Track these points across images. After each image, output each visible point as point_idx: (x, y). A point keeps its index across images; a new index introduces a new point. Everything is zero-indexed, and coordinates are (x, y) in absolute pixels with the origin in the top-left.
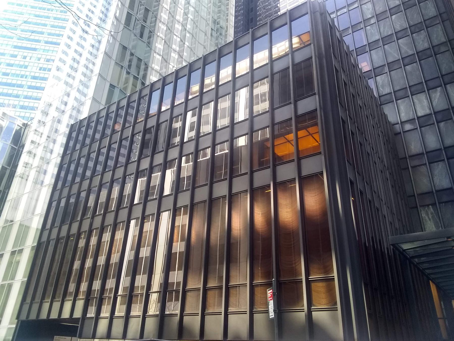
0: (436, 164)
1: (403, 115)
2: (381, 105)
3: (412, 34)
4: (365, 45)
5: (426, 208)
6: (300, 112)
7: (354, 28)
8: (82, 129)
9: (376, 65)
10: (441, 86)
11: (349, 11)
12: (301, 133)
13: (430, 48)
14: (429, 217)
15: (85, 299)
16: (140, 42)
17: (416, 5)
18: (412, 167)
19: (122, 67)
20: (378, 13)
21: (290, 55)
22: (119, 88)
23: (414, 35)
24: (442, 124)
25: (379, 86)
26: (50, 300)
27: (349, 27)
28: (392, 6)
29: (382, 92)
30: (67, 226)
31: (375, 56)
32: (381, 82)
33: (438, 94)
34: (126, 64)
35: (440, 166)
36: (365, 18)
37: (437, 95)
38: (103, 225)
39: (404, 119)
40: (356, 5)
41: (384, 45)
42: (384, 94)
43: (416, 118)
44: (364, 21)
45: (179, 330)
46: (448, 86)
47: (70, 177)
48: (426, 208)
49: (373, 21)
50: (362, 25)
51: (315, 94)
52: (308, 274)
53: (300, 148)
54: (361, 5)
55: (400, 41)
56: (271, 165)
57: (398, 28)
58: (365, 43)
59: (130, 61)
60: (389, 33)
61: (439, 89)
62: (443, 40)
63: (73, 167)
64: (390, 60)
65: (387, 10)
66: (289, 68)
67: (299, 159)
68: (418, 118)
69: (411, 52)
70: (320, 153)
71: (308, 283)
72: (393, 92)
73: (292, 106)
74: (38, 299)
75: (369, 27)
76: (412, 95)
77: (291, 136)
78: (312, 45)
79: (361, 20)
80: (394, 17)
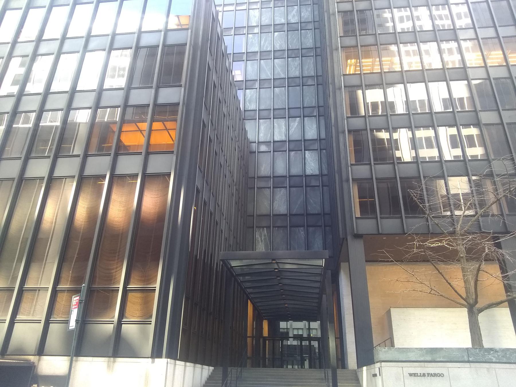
1: (261, 135)
2: (244, 119)
3: (288, 58)
6: (161, 101)
7: (237, 30)
9: (249, 78)
10: (300, 117)
11: (236, 10)
12: (156, 125)
13: (299, 77)
17: (298, 30)
20: (263, 24)
21: (163, 33)
23: (290, 59)
24: (292, 153)
25: (247, 100)
27: (232, 28)
28: (277, 23)
33: (296, 124)
35: (282, 192)
36: (250, 24)
37: (295, 124)
39: (261, 140)
40: (244, 7)
41: (260, 59)
42: (249, 109)
43: (272, 141)
44: (248, 27)
46: (306, 119)
49: (256, 30)
50: (245, 31)
51: (181, 86)
53: (153, 141)
54: (249, 9)
55: (276, 60)
56: (113, 152)
57: (278, 47)
58: (244, 51)
60: (269, 49)
61: (298, 119)
62: (312, 73)
64: (263, 77)
65: (272, 25)
66: (158, 46)
67: (148, 154)
69: (283, 76)
70: (172, 152)
72: (258, 110)
73: (153, 91)
75: (251, 35)
76: (273, 118)
77: (144, 126)
78: (190, 31)
79: (245, 25)
80: (276, 34)
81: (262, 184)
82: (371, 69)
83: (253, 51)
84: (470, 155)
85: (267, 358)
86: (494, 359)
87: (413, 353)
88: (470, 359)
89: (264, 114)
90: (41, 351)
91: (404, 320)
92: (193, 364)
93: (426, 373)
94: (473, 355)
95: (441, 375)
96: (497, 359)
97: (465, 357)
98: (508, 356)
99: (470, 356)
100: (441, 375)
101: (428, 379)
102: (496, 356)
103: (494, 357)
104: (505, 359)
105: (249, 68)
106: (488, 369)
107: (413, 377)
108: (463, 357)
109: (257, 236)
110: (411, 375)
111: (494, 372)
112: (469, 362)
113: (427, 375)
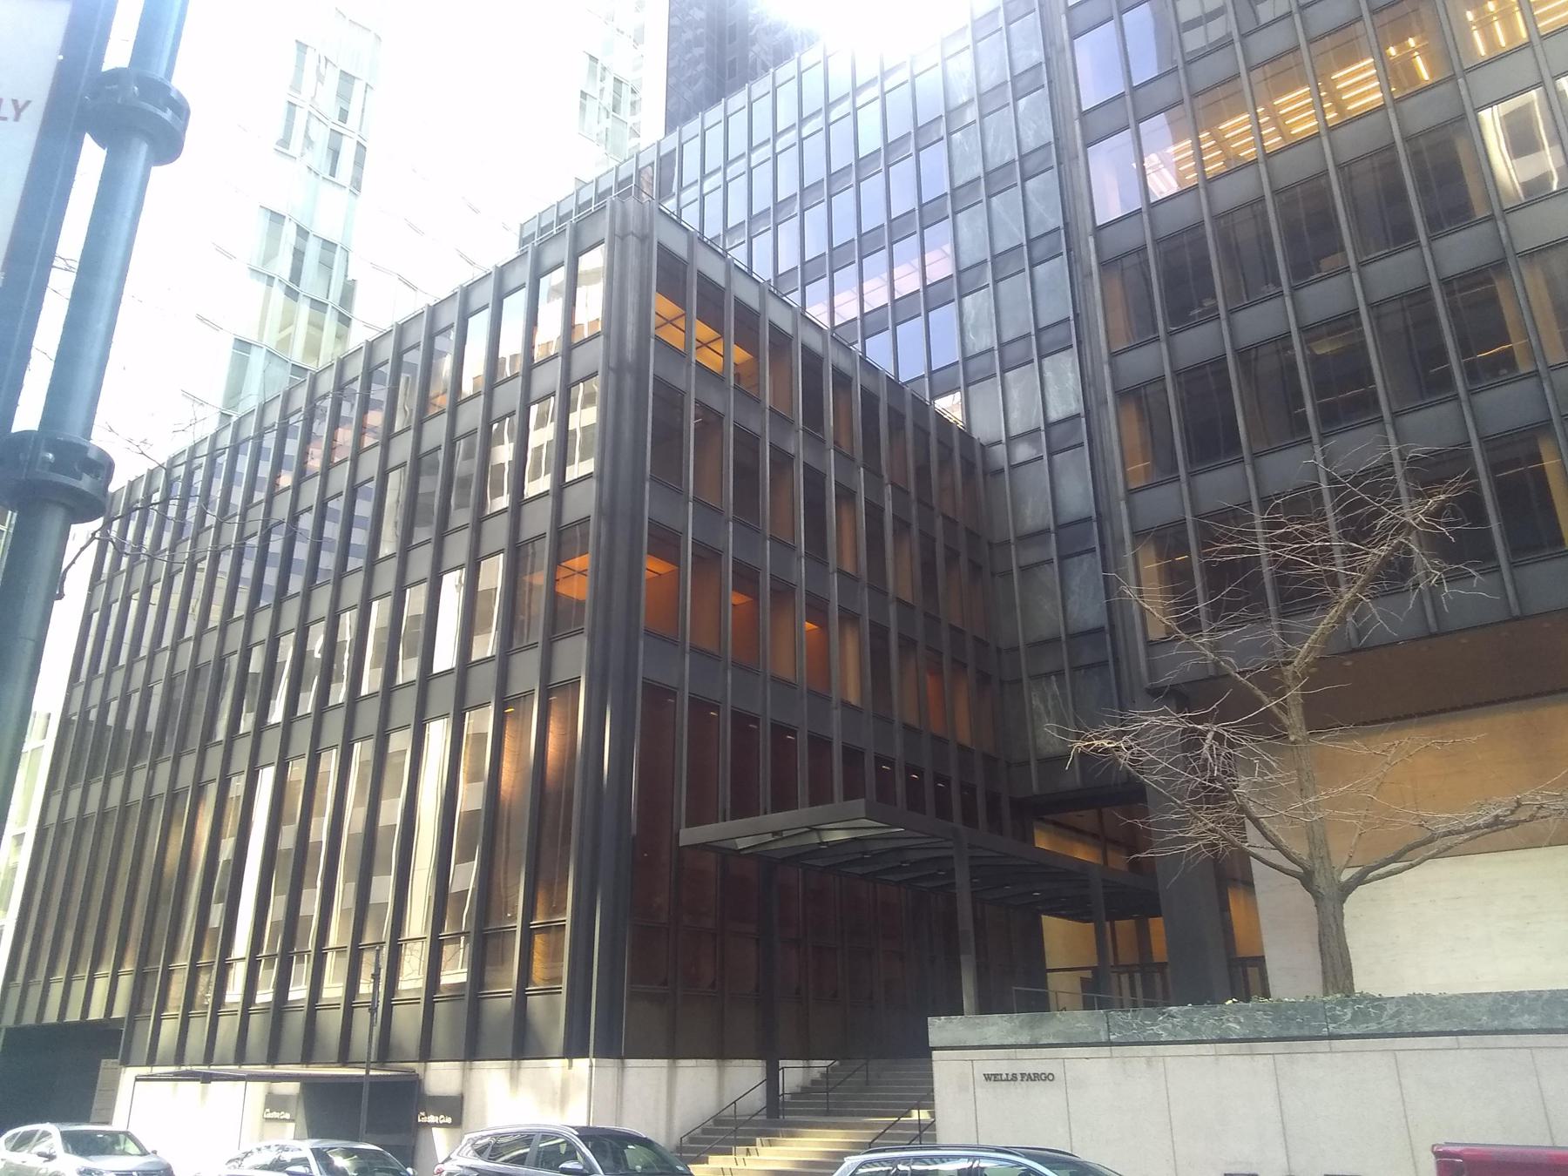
0: (1076, 559)
1: (1015, 415)
4: (1007, 164)
5: (1044, 683)
8: (219, 460)
14: (1046, 707)
15: (134, 973)
16: (330, 185)
18: (1024, 569)
19: (271, 278)
22: (265, 348)
25: (968, 327)
26: (87, 974)
29: (974, 345)
30: (79, 791)
31: (965, 230)
32: (973, 312)
34: (283, 267)
35: (1085, 566)
38: (150, 792)
45: (305, 1041)
47: (271, 576)
48: (1044, 683)
52: (529, 913)
59: (299, 255)
60: (1007, 158)
63: (276, 546)
68: (1049, 425)
71: (528, 935)
74: (41, 976)
75: (959, 133)
81: (1032, 555)
82: (1251, 128)
83: (969, 179)
84: (5, 928)
85: (367, 1072)
86: (1164, 1034)
87: (995, 1028)
88: (1112, 1037)
89: (1013, 353)
90: (426, 1055)
91: (1372, 900)
92: (713, 1062)
93: (1018, 1072)
94: (1120, 1027)
95: (1047, 1077)
96: (1170, 1034)
97: (1102, 1033)
98: (1195, 1025)
99: (1112, 1029)
100: (1047, 1077)
101: (1021, 1087)
102: (1170, 1026)
103: (1164, 1029)
104: (1187, 1033)
105: (964, 233)
106: (1149, 1059)
107: (992, 1084)
108: (1097, 1032)
109: (1036, 702)
110: (988, 1077)
111: (1161, 1064)
112: (1110, 1044)
113: (1019, 1078)
